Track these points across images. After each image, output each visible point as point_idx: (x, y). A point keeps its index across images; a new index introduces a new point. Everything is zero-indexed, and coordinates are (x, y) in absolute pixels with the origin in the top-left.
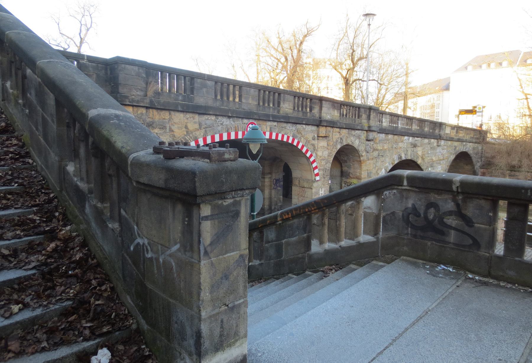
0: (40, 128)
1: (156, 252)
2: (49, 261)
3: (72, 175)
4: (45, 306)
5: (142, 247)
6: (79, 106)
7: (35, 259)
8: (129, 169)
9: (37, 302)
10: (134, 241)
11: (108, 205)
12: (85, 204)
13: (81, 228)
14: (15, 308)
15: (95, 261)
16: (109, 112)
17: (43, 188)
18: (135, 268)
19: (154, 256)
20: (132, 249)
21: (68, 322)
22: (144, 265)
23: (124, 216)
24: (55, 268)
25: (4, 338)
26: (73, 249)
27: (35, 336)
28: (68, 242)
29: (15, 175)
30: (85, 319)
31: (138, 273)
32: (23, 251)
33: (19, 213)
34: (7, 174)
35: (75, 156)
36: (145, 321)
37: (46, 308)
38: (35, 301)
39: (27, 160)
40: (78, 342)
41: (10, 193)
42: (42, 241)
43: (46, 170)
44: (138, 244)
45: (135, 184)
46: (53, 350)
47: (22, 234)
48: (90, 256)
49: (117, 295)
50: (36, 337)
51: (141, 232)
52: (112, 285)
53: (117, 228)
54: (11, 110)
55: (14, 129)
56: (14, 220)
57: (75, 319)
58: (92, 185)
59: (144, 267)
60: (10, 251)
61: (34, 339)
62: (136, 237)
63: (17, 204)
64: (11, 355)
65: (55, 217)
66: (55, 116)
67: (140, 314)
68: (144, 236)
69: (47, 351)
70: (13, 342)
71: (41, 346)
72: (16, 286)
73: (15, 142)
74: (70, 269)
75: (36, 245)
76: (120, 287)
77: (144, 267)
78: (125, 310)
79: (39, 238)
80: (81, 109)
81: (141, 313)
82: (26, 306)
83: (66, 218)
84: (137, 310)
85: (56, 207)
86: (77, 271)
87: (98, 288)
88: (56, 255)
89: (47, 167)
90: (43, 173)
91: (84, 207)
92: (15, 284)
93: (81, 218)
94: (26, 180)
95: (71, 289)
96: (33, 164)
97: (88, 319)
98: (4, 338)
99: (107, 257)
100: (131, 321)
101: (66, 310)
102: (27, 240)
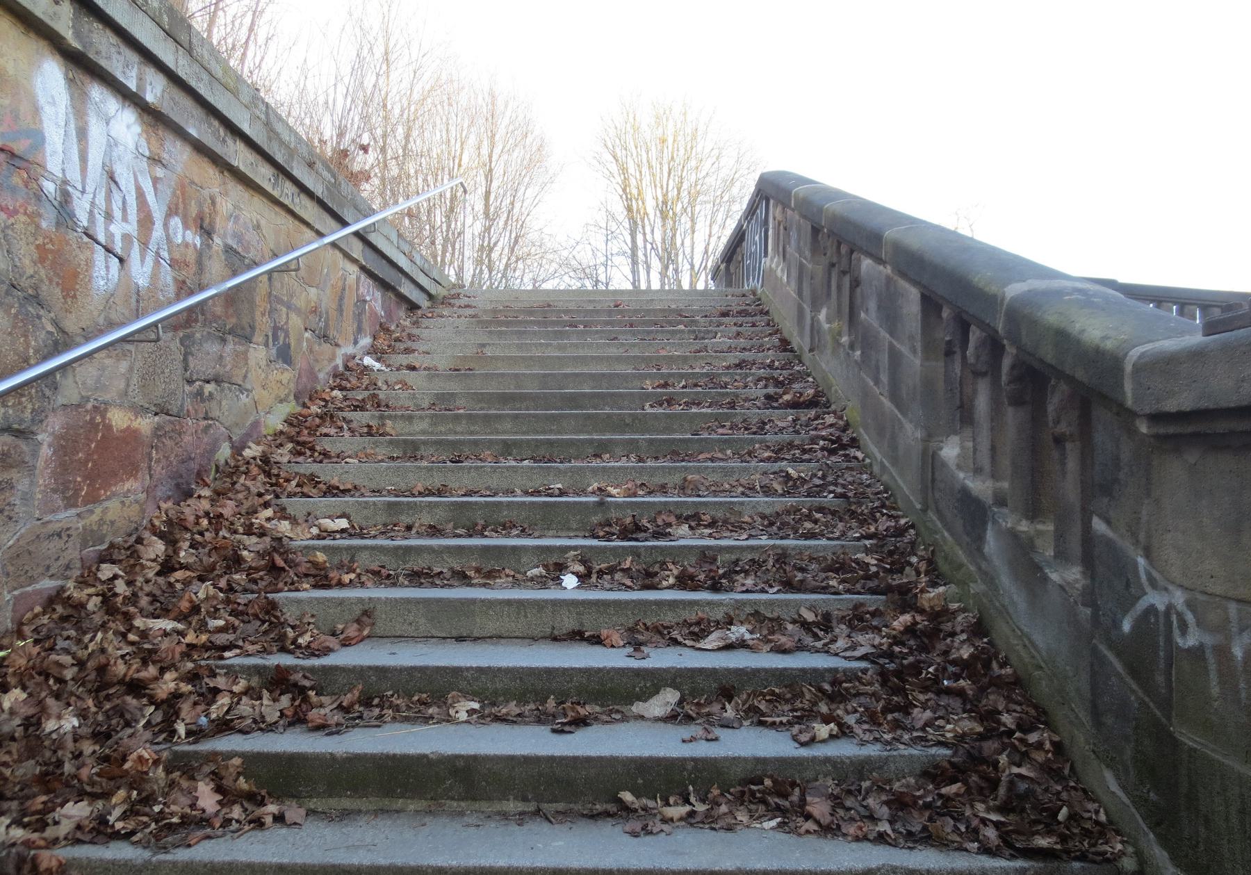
0: (884, 378)
1: (1222, 628)
2: (897, 649)
3: (954, 468)
4: (887, 743)
5: (1162, 620)
6: (980, 285)
7: (867, 642)
8: (1128, 387)
9: (870, 731)
10: (1133, 604)
11: (1050, 527)
12: (985, 530)
13: (972, 592)
14: (823, 730)
15: (1009, 670)
16: (1056, 285)
17: (883, 506)
18: (1134, 686)
19: (1209, 640)
20: (1126, 626)
21: (941, 796)
22: (1171, 674)
23: (1103, 536)
24: (911, 665)
25: (798, 785)
26: (953, 634)
27: (864, 803)
28: (940, 620)
29: (830, 479)
30: (983, 802)
31: (1147, 699)
32: (842, 620)
33: (835, 546)
34: (814, 475)
35: (964, 416)
36: (1165, 854)
37: (888, 748)
38: (866, 726)
39: (853, 452)
40: (966, 850)
41: (821, 509)
42: (881, 608)
43: (891, 469)
44: (1151, 610)
45: (1144, 428)
46: (903, 847)
47: (841, 587)
48: (996, 656)
49: (1072, 768)
50: (865, 807)
51: (1161, 573)
52: (1056, 738)
53: (1076, 581)
54: (824, 366)
55: (828, 401)
56: (825, 559)
57: (957, 795)
58: (1005, 485)
59: (1169, 679)
60: (816, 616)
61: (861, 809)
62: (1143, 590)
63: (832, 533)
64: (810, 825)
65: (911, 564)
66: (919, 337)
67: (1150, 828)
68: (1173, 583)
69: (890, 844)
70: (817, 800)
71: (877, 829)
72: (827, 687)
73: (830, 419)
74: (946, 675)
75: (868, 612)
76: (1081, 741)
77: (1169, 679)
78: (1097, 812)
79: (876, 601)
80: (987, 289)
81: (1155, 825)
82: (844, 731)
83: (935, 570)
84: (1138, 816)
85: (913, 544)
86: (962, 683)
87: (1017, 734)
88: (912, 642)
89: (895, 461)
90: (885, 478)
91: (980, 539)
92: (825, 681)
93: (972, 568)
94: (851, 490)
95: (948, 722)
96: (863, 460)
97: (991, 803)
98: (798, 785)
99: (1043, 665)
100: (1119, 847)
101: (936, 767)
102: (852, 600)
